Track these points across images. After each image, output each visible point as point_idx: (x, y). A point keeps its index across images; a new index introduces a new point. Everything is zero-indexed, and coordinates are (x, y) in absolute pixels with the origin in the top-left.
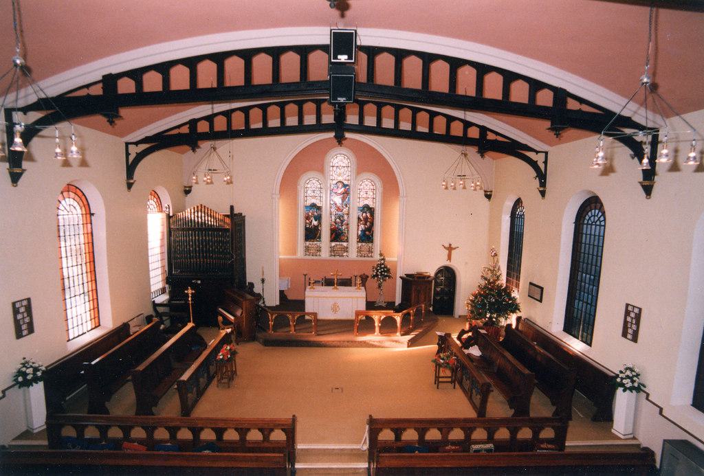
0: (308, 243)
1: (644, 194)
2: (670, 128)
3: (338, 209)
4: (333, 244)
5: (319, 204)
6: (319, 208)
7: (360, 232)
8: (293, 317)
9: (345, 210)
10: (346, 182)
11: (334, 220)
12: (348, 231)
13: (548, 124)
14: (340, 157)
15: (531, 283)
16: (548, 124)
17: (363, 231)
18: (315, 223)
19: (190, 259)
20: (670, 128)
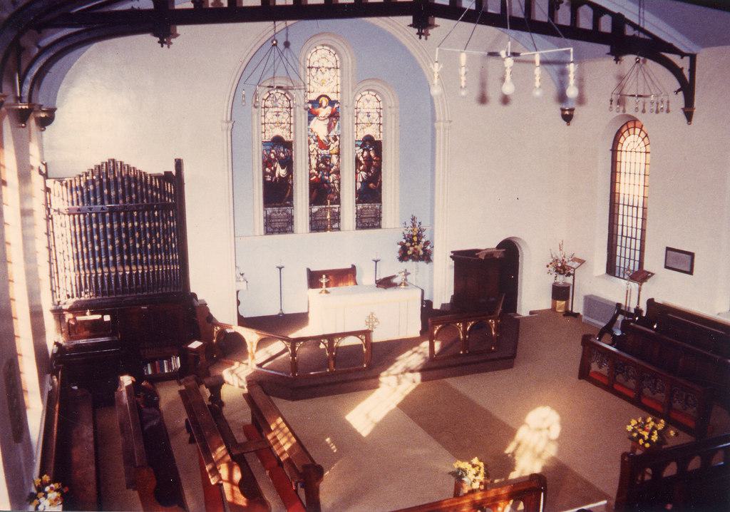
0: (269, 210)
1: (686, 121)
2: (706, 58)
3: (323, 145)
4: (315, 209)
5: (287, 139)
6: (288, 145)
7: (359, 185)
8: (465, 327)
9: (333, 146)
10: (333, 97)
11: (314, 166)
12: (339, 184)
13: (607, 48)
14: (323, 52)
15: (668, 249)
16: (607, 48)
17: (365, 182)
18: (281, 172)
19: (95, 268)
20: (706, 58)
